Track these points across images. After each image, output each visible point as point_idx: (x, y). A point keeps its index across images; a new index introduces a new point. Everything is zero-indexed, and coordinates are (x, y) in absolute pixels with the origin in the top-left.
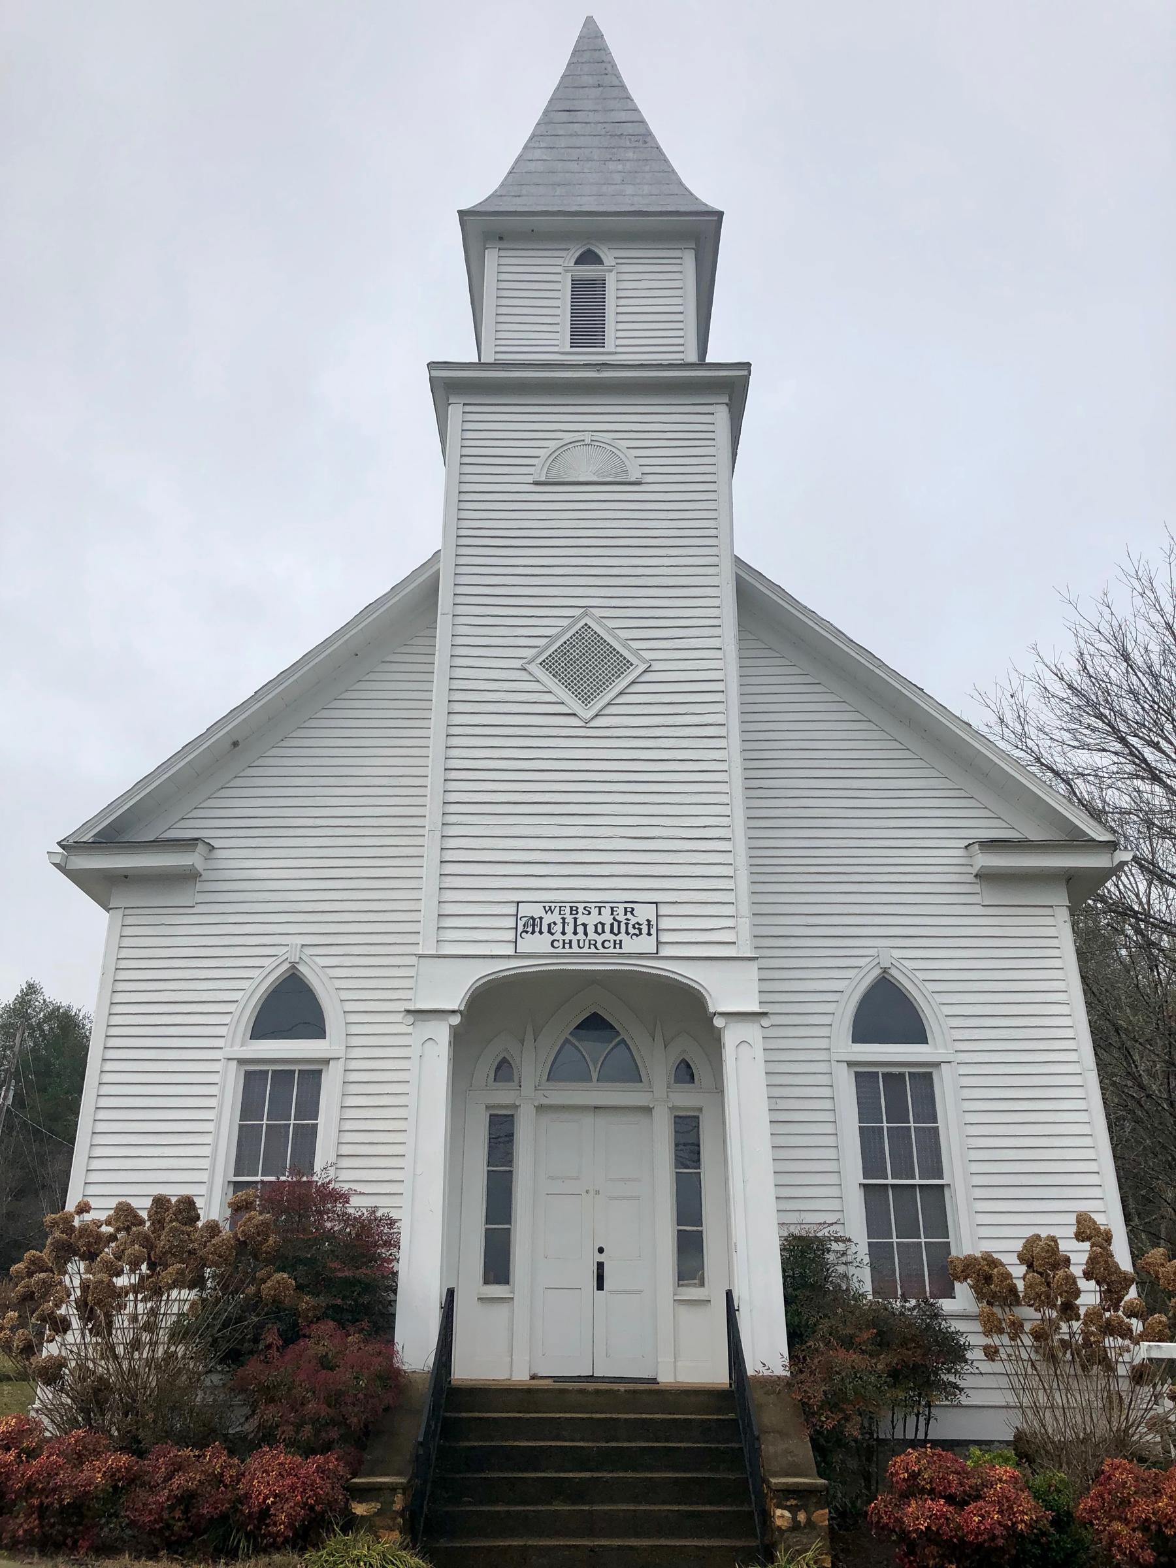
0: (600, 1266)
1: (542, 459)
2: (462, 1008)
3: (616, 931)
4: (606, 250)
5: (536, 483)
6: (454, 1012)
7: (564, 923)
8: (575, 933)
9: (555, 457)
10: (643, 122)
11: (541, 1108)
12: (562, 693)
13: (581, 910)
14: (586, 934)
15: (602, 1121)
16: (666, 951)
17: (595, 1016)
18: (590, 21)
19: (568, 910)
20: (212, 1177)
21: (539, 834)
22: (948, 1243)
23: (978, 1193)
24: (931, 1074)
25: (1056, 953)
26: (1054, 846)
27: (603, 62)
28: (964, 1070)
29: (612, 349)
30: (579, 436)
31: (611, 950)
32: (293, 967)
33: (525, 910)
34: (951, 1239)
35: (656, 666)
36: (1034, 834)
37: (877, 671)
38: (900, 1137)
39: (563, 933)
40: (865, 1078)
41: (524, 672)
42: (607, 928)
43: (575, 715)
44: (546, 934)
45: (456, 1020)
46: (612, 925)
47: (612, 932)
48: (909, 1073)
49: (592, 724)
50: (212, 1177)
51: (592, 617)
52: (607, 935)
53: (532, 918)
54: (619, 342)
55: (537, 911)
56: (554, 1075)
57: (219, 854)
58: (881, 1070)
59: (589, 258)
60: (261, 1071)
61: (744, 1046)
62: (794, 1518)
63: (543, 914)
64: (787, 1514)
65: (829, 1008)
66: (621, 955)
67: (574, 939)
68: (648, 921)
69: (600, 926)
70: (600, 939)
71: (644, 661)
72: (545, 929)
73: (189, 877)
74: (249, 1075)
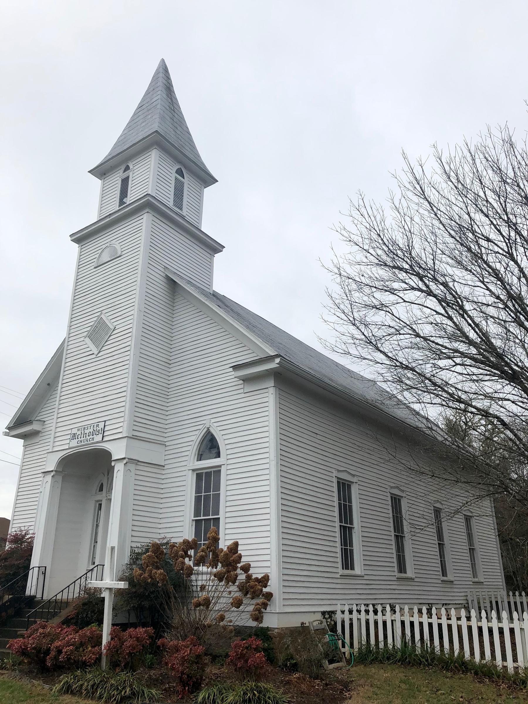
5: (95, 268)
6: (52, 471)
18: (163, 60)
26: (263, 361)
30: (107, 245)
32: (208, 429)
57: (46, 423)
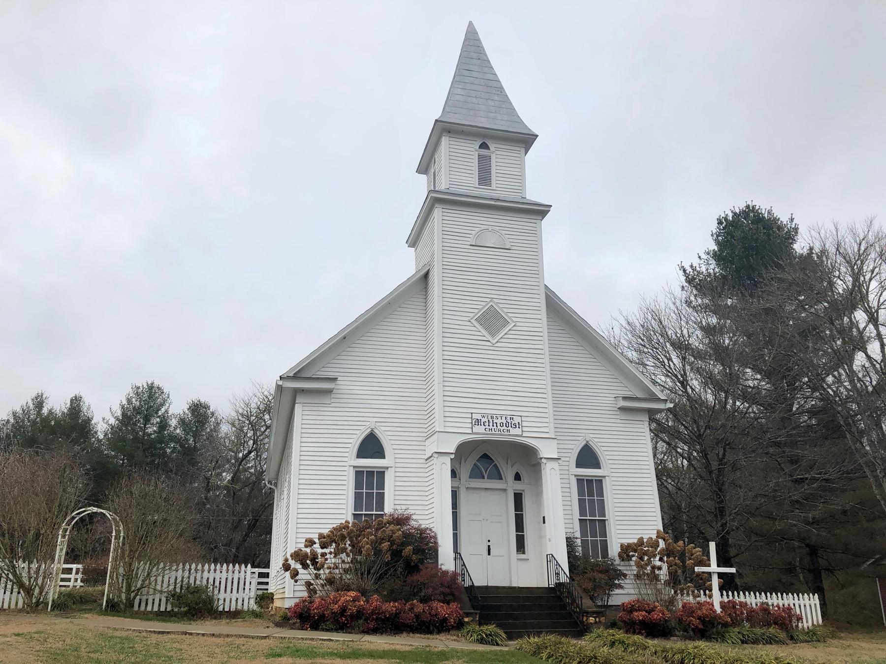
0: (489, 546)
2: (454, 452)
3: (507, 426)
4: (491, 143)
5: (471, 245)
6: (452, 453)
7: (489, 422)
8: (493, 426)
9: (478, 236)
11: (467, 488)
12: (484, 332)
13: (495, 417)
14: (497, 426)
15: (488, 493)
17: (485, 454)
18: (471, 24)
19: (490, 417)
22: (607, 540)
23: (618, 523)
24: (602, 480)
25: (644, 438)
27: (479, 47)
28: (613, 479)
29: (495, 188)
31: (506, 433)
33: (475, 416)
35: (518, 324)
36: (639, 395)
37: (588, 329)
38: (592, 502)
39: (489, 426)
42: (504, 425)
43: (489, 341)
45: (453, 456)
46: (506, 423)
47: (506, 426)
48: (595, 480)
51: (494, 302)
52: (504, 427)
53: (477, 419)
54: (497, 185)
55: (479, 417)
58: (585, 478)
59: (484, 146)
60: (361, 471)
62: (595, 620)
63: (481, 418)
64: (593, 619)
66: (510, 435)
68: (519, 423)
69: (502, 424)
70: (502, 429)
72: (482, 424)
73: (329, 392)
74: (357, 472)
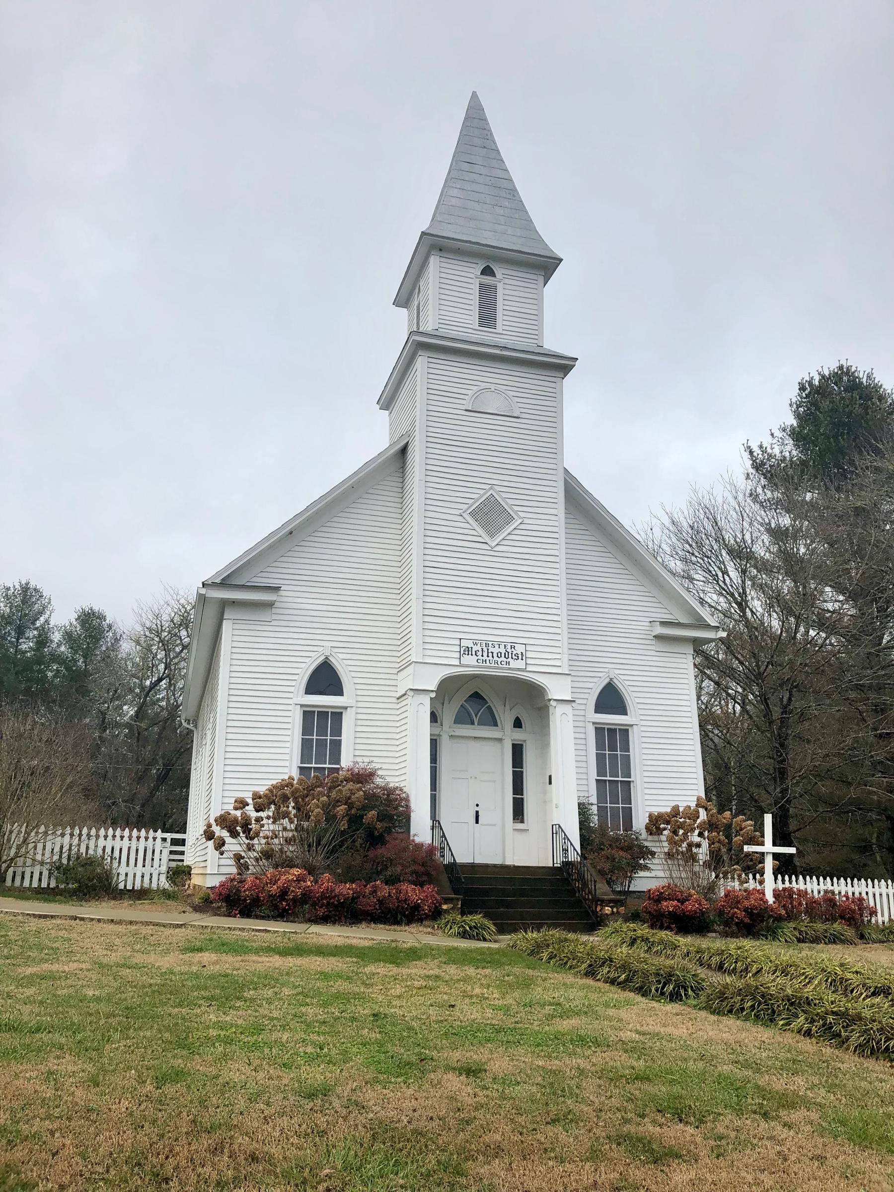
0: (477, 812)
1: (470, 395)
5: (466, 410)
8: (488, 656)
9: (477, 397)
10: (511, 180)
12: (481, 531)
13: (490, 645)
14: (493, 657)
16: (530, 668)
18: (474, 95)
19: (484, 645)
20: (291, 764)
21: (470, 604)
28: (643, 729)
31: (505, 666)
33: (464, 643)
34: (633, 806)
35: (526, 521)
38: (614, 758)
39: (482, 656)
40: (599, 730)
41: (461, 517)
44: (474, 656)
45: (433, 695)
49: (495, 549)
50: (291, 764)
52: (503, 659)
56: (458, 720)
59: (487, 271)
61: (564, 715)
63: (473, 646)
65: (586, 696)
66: (510, 669)
67: (488, 659)
70: (499, 660)
71: (521, 518)
72: (474, 653)
73: (269, 605)
74: (305, 713)
